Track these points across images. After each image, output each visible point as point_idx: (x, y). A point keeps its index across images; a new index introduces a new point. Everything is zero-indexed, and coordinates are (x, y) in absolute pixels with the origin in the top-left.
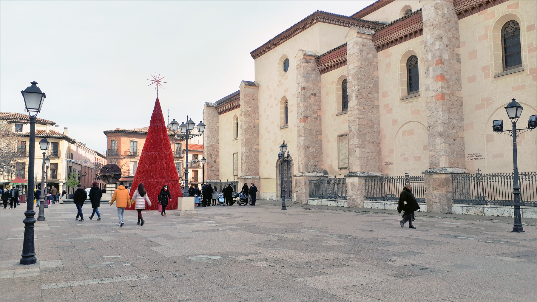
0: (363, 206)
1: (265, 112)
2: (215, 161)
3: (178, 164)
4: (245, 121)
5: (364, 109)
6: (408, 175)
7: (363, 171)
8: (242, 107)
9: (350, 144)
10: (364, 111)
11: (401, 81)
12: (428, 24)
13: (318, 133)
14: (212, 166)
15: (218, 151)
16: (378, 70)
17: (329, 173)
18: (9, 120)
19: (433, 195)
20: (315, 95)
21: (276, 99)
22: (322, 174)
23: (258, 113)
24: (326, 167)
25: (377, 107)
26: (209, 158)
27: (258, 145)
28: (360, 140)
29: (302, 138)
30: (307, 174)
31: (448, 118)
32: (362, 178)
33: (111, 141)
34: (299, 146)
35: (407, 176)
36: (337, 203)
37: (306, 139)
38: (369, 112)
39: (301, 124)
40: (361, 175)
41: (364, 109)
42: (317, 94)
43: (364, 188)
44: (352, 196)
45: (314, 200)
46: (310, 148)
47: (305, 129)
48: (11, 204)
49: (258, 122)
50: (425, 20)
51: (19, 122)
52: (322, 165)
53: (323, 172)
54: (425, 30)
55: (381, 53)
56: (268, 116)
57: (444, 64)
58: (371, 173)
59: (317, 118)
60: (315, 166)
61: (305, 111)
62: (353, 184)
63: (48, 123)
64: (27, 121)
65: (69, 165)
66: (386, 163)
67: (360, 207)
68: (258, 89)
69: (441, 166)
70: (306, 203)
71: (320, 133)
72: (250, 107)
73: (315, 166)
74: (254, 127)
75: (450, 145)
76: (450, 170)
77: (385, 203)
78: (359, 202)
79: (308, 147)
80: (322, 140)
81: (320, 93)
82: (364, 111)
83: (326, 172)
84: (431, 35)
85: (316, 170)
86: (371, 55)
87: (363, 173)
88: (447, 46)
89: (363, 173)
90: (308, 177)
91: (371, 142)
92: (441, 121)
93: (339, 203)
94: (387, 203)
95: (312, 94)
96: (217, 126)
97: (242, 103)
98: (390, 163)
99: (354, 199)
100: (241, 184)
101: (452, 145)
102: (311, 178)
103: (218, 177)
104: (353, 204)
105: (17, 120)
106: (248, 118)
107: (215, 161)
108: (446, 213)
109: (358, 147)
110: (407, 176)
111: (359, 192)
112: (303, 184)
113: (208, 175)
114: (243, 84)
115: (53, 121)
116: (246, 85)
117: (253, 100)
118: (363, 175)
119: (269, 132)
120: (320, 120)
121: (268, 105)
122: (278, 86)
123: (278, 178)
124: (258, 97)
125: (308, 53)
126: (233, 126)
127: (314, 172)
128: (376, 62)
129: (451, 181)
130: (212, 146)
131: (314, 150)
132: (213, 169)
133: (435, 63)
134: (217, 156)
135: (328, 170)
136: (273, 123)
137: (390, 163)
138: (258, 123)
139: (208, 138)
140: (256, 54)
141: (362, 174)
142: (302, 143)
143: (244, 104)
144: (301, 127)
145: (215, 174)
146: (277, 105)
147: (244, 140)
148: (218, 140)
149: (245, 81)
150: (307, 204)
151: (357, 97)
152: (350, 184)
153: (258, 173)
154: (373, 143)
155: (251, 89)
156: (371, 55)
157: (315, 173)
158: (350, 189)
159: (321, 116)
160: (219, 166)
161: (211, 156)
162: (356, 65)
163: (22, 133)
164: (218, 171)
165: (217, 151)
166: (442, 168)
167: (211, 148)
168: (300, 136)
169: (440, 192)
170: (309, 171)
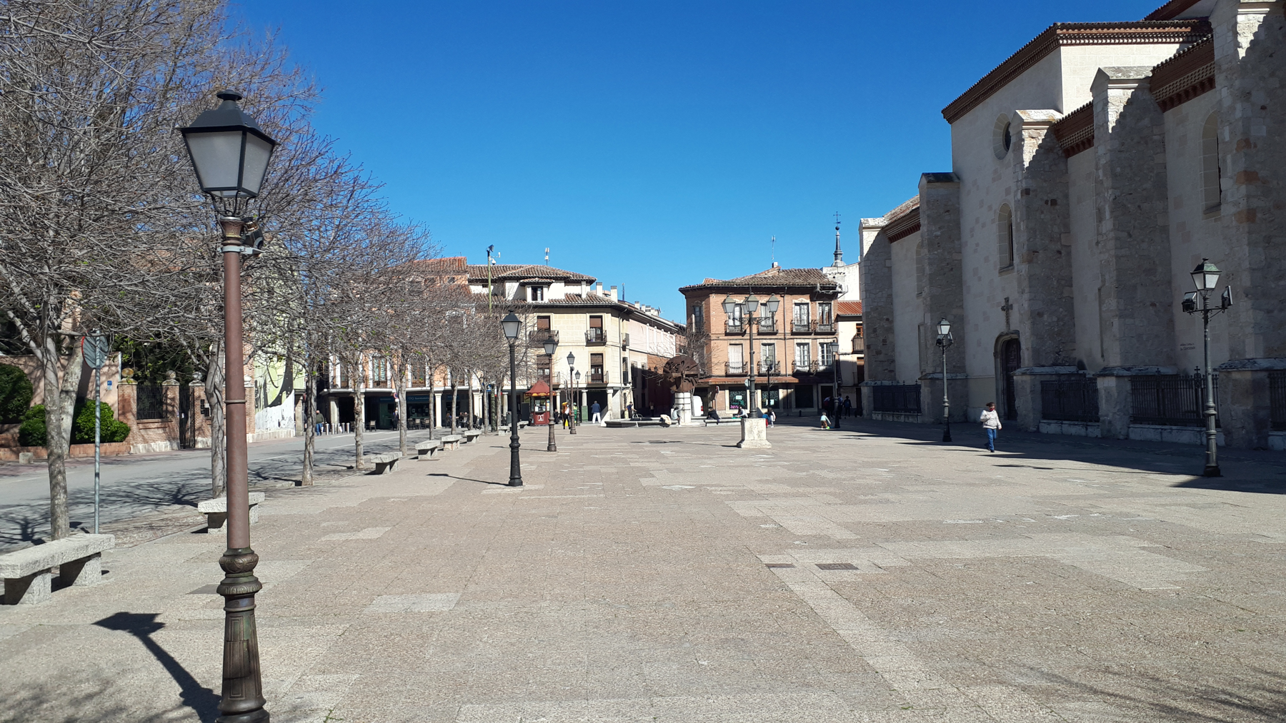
0: (1128, 435)
1: (972, 236)
2: (884, 341)
3: (825, 345)
4: (929, 258)
5: (1130, 236)
6: (1199, 372)
7: (1128, 365)
8: (923, 229)
9: (1104, 309)
10: (1129, 240)
11: (1205, 173)
12: (1224, 67)
13: (1063, 282)
14: (879, 353)
15: (890, 319)
16: (1165, 151)
17: (1087, 367)
18: (521, 281)
19: (1233, 413)
20: (1054, 202)
21: (990, 208)
22: (1073, 369)
23: (959, 239)
24: (1080, 354)
25: (1165, 229)
26: (872, 335)
27: (961, 307)
28: (940, 333)
29: (1026, 296)
30: (1038, 370)
31: (1264, 257)
32: (1126, 379)
33: (693, 306)
34: (1022, 312)
35: (1197, 374)
36: (1087, 429)
37: (1035, 297)
38: (1143, 241)
39: (1023, 266)
40: (1122, 372)
41: (1130, 236)
42: (1059, 201)
43: (1129, 399)
44: (1107, 416)
45: (1049, 424)
46: (1045, 316)
47: (1031, 277)
48: (834, 288)
49: (959, 258)
50: (1218, 58)
51: (538, 283)
52: (1075, 350)
53: (1076, 364)
54: (1220, 80)
55: (1169, 115)
56: (977, 245)
57: (1255, 146)
58: (1147, 367)
59: (1059, 252)
60: (1057, 353)
61: (1031, 240)
62: (1108, 391)
63: (584, 280)
64: (549, 280)
65: (622, 356)
66: (1182, 347)
67: (1121, 437)
68: (959, 188)
69: (1248, 357)
70: (1035, 429)
71: (1069, 282)
72: (940, 228)
73: (1057, 353)
74: (952, 269)
75: (1269, 312)
76: (1265, 364)
77: (1162, 429)
78: (1118, 427)
79: (1040, 315)
80: (1072, 298)
81: (1066, 196)
82: (1129, 240)
83: (1081, 365)
84: (1228, 89)
85: (1060, 361)
86: (1146, 121)
87: (1128, 369)
88: (1263, 108)
89: (1128, 369)
90: (1038, 377)
91: (1148, 304)
92: (1246, 264)
93: (1090, 429)
94: (1165, 429)
95: (1046, 202)
96: (888, 267)
97: (923, 221)
98: (1189, 346)
99: (1110, 422)
100: (926, 390)
101: (1276, 312)
102: (1047, 378)
103: (893, 374)
104: (1109, 431)
105: (534, 280)
106: (936, 252)
107: (884, 341)
108: (1255, 449)
109: (1117, 316)
110: (1197, 374)
111: (1118, 408)
112: (1028, 391)
113: (869, 371)
114: (924, 181)
115: (592, 277)
116: (929, 182)
117: (948, 211)
118: (1126, 373)
119: (980, 279)
120: (1069, 254)
121: (977, 221)
122: (994, 180)
123: (999, 376)
124: (959, 204)
125: (1035, 118)
126: (917, 267)
127: (1054, 365)
128: (1160, 135)
129: (1268, 385)
130: (877, 309)
131: (1055, 319)
132: (881, 357)
133: (1235, 146)
134: (890, 330)
135: (1085, 361)
136: (987, 260)
137: (1189, 346)
138: (961, 260)
139: (868, 294)
140: (953, 113)
141: (1125, 372)
142: (1026, 305)
143: (926, 222)
144: (1023, 272)
145: (887, 369)
146: (993, 221)
147: (928, 299)
148: (890, 296)
149: (929, 174)
150: (1038, 431)
151: (1112, 212)
152: (1103, 391)
153: (964, 367)
154: (1153, 305)
155: (941, 189)
156: (1146, 121)
157: (1057, 368)
158: (1104, 401)
159: (1070, 246)
160: (893, 350)
161: (875, 330)
162: (1109, 148)
163: (543, 302)
164: (893, 361)
165: (887, 319)
166: (1249, 360)
167: (875, 315)
168: (1023, 292)
169: (1243, 408)
170: (1043, 363)
